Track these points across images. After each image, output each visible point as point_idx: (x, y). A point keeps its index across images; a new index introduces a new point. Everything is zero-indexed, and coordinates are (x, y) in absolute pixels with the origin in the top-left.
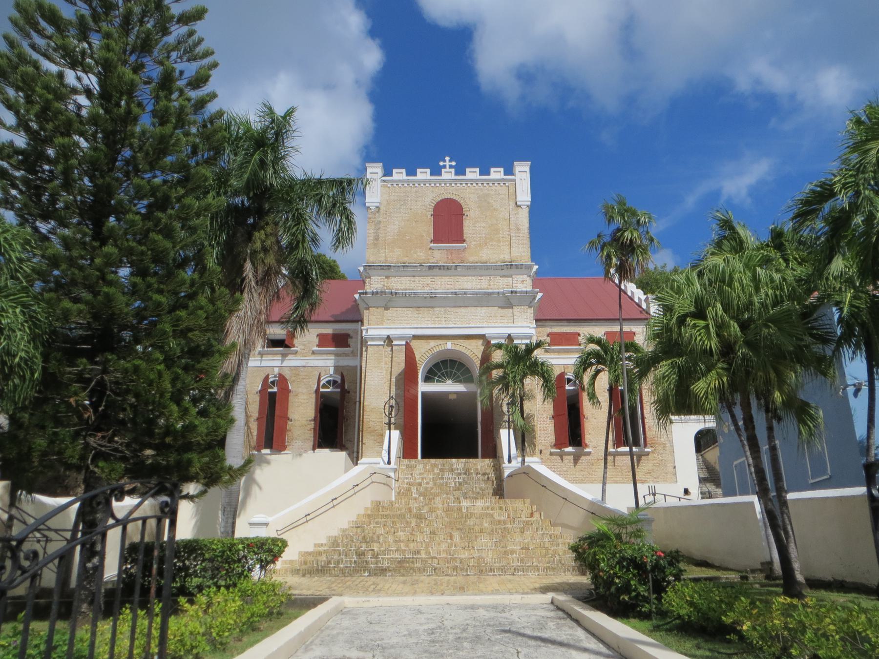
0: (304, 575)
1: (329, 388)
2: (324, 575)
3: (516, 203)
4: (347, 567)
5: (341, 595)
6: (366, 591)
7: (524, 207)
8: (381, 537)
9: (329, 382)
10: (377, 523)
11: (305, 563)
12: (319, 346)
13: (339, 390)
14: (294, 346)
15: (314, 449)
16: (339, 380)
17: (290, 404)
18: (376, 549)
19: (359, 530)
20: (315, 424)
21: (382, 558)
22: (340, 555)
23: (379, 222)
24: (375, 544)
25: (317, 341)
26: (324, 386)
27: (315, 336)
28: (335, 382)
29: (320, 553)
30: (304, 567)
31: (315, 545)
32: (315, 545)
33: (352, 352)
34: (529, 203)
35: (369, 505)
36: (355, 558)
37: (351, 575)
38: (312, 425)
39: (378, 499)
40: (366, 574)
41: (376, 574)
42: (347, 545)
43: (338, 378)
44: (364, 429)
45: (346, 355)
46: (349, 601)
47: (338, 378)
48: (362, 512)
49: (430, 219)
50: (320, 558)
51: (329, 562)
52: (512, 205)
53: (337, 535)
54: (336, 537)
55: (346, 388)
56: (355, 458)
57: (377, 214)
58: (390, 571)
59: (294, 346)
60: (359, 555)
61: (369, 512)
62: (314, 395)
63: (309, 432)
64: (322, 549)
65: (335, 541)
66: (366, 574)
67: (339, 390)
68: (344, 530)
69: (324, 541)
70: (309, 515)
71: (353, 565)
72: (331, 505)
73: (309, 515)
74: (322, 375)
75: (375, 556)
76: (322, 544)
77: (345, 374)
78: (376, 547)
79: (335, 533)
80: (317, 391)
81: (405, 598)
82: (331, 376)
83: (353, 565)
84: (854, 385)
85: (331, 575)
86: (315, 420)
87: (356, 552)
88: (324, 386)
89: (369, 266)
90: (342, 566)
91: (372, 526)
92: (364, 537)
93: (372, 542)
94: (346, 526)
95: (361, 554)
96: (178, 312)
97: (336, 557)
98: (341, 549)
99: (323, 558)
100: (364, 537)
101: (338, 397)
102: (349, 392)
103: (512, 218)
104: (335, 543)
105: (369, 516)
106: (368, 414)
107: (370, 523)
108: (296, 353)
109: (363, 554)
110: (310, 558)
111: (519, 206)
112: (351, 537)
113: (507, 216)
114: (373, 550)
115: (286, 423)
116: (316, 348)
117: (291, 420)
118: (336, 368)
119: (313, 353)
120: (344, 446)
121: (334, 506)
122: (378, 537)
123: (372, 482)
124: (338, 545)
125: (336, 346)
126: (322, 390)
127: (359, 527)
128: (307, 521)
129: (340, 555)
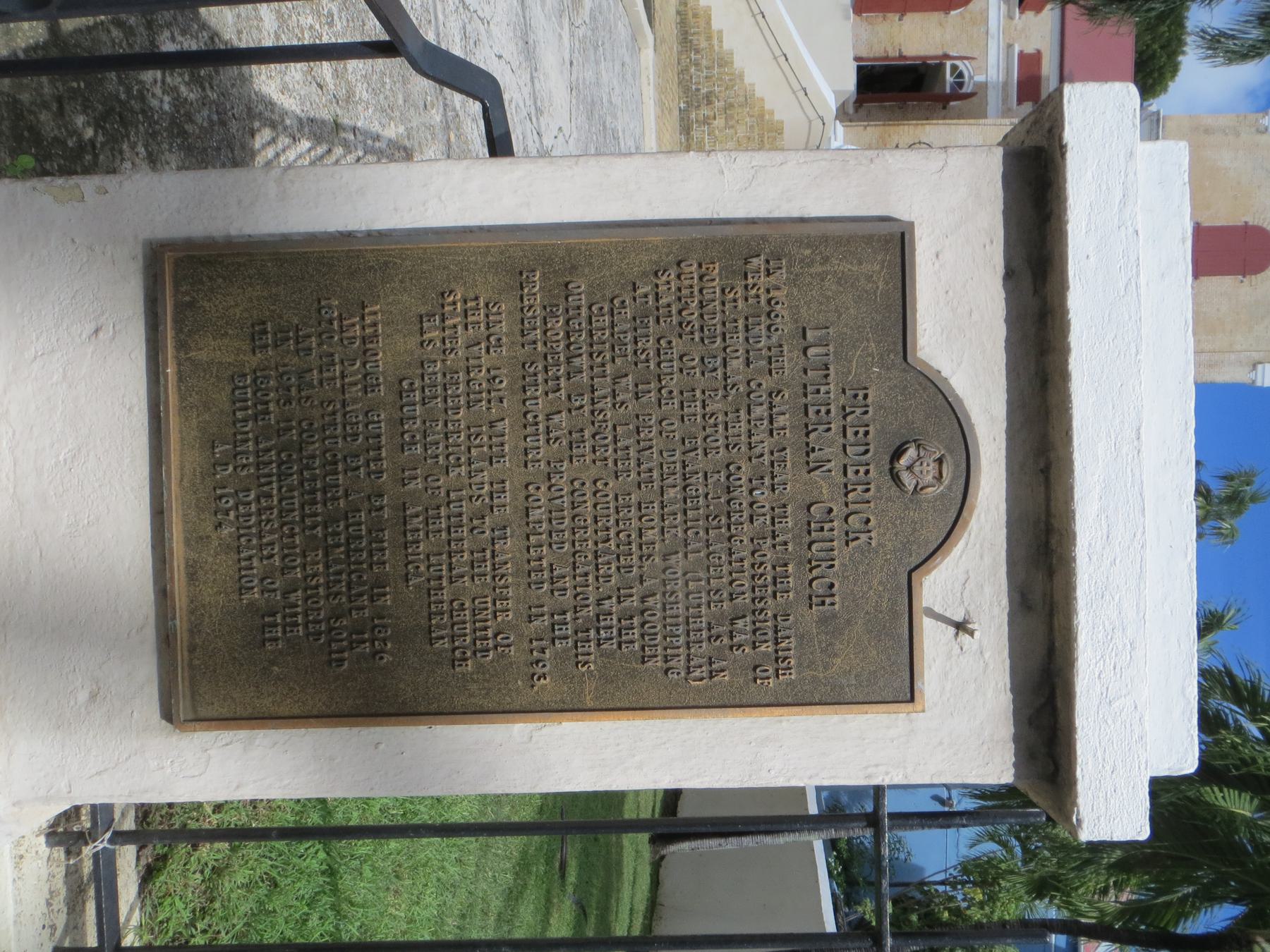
0: (678, 13)
1: (951, 75)
2: (680, 43)
3: (1260, 363)
4: (691, 77)
5: (655, 50)
6: (660, 104)
7: (1252, 375)
8: (732, 131)
9: (961, 75)
10: (752, 127)
11: (695, 16)
12: (1021, 55)
13: (948, 90)
14: (1022, 12)
15: (857, 59)
16: (966, 90)
17: (926, 15)
18: (716, 122)
19: (742, 99)
20: (894, 59)
21: (704, 131)
22: (707, 68)
23: (1238, 134)
24: (723, 121)
25: (1030, 50)
26: (954, 68)
27: (1039, 47)
28: (961, 85)
29: (709, 38)
30: (690, 14)
31: (720, 32)
32: (720, 32)
33: (1009, 110)
34: (1259, 383)
35: (777, 117)
36: (704, 91)
37: (680, 83)
38: (893, 53)
39: (785, 135)
40: (682, 105)
41: (682, 119)
42: (721, 79)
43: (967, 89)
44: (887, 128)
45: (1005, 100)
46: (648, 56)
47: (967, 89)
48: (767, 107)
49: (1238, 220)
50: (702, 38)
51: (697, 51)
52: (1256, 356)
53: (735, 66)
54: (732, 63)
55: (952, 103)
56: (843, 114)
57: (1253, 130)
58: (688, 140)
59: (1022, 12)
60: (707, 97)
61: (767, 117)
62: (940, 53)
63: (882, 50)
64: (715, 42)
65: (726, 63)
66: (682, 105)
67: (948, 90)
68: (741, 76)
69: (726, 46)
70: (764, 17)
71: (694, 87)
72: (778, 53)
73: (764, 17)
74: (974, 62)
75: (706, 121)
76: (721, 42)
77: (974, 99)
78: (719, 122)
79: (738, 63)
80: (947, 57)
81: (654, 136)
82: (971, 77)
83: (694, 87)
84: (950, 798)
85: (680, 53)
86: (902, 57)
87: (711, 92)
88: (954, 68)
89: (1158, 120)
90: (693, 70)
91: (748, 119)
92: (731, 106)
93: (726, 118)
94: (747, 80)
95: (709, 98)
96: (1016, 121)
97: (704, 62)
98: (716, 71)
99: (703, 44)
100: (731, 106)
101: (937, 90)
102: (944, 108)
103: (1233, 357)
104: (724, 61)
105: (762, 116)
106: (911, 132)
107: (753, 116)
108: (1011, 17)
109: (709, 103)
110: (702, 24)
111: (1254, 366)
112: (733, 86)
113: (1238, 347)
114: (715, 118)
115: (896, 11)
116: (1017, 49)
117: (900, 20)
118: (984, 86)
119: (1010, 46)
120: (861, 106)
121: (775, 58)
122: (732, 127)
123: (810, 122)
124: (720, 66)
125: (1019, 83)
126: (948, 64)
127: (746, 99)
128: (754, 16)
129: (707, 68)
